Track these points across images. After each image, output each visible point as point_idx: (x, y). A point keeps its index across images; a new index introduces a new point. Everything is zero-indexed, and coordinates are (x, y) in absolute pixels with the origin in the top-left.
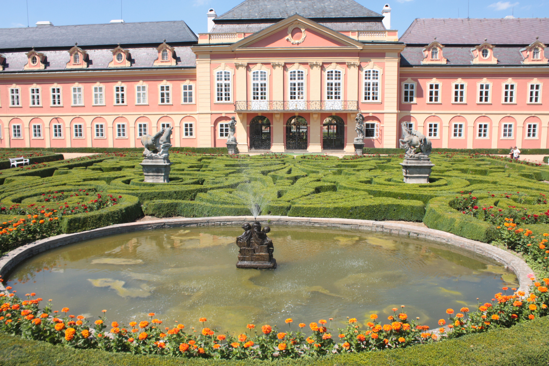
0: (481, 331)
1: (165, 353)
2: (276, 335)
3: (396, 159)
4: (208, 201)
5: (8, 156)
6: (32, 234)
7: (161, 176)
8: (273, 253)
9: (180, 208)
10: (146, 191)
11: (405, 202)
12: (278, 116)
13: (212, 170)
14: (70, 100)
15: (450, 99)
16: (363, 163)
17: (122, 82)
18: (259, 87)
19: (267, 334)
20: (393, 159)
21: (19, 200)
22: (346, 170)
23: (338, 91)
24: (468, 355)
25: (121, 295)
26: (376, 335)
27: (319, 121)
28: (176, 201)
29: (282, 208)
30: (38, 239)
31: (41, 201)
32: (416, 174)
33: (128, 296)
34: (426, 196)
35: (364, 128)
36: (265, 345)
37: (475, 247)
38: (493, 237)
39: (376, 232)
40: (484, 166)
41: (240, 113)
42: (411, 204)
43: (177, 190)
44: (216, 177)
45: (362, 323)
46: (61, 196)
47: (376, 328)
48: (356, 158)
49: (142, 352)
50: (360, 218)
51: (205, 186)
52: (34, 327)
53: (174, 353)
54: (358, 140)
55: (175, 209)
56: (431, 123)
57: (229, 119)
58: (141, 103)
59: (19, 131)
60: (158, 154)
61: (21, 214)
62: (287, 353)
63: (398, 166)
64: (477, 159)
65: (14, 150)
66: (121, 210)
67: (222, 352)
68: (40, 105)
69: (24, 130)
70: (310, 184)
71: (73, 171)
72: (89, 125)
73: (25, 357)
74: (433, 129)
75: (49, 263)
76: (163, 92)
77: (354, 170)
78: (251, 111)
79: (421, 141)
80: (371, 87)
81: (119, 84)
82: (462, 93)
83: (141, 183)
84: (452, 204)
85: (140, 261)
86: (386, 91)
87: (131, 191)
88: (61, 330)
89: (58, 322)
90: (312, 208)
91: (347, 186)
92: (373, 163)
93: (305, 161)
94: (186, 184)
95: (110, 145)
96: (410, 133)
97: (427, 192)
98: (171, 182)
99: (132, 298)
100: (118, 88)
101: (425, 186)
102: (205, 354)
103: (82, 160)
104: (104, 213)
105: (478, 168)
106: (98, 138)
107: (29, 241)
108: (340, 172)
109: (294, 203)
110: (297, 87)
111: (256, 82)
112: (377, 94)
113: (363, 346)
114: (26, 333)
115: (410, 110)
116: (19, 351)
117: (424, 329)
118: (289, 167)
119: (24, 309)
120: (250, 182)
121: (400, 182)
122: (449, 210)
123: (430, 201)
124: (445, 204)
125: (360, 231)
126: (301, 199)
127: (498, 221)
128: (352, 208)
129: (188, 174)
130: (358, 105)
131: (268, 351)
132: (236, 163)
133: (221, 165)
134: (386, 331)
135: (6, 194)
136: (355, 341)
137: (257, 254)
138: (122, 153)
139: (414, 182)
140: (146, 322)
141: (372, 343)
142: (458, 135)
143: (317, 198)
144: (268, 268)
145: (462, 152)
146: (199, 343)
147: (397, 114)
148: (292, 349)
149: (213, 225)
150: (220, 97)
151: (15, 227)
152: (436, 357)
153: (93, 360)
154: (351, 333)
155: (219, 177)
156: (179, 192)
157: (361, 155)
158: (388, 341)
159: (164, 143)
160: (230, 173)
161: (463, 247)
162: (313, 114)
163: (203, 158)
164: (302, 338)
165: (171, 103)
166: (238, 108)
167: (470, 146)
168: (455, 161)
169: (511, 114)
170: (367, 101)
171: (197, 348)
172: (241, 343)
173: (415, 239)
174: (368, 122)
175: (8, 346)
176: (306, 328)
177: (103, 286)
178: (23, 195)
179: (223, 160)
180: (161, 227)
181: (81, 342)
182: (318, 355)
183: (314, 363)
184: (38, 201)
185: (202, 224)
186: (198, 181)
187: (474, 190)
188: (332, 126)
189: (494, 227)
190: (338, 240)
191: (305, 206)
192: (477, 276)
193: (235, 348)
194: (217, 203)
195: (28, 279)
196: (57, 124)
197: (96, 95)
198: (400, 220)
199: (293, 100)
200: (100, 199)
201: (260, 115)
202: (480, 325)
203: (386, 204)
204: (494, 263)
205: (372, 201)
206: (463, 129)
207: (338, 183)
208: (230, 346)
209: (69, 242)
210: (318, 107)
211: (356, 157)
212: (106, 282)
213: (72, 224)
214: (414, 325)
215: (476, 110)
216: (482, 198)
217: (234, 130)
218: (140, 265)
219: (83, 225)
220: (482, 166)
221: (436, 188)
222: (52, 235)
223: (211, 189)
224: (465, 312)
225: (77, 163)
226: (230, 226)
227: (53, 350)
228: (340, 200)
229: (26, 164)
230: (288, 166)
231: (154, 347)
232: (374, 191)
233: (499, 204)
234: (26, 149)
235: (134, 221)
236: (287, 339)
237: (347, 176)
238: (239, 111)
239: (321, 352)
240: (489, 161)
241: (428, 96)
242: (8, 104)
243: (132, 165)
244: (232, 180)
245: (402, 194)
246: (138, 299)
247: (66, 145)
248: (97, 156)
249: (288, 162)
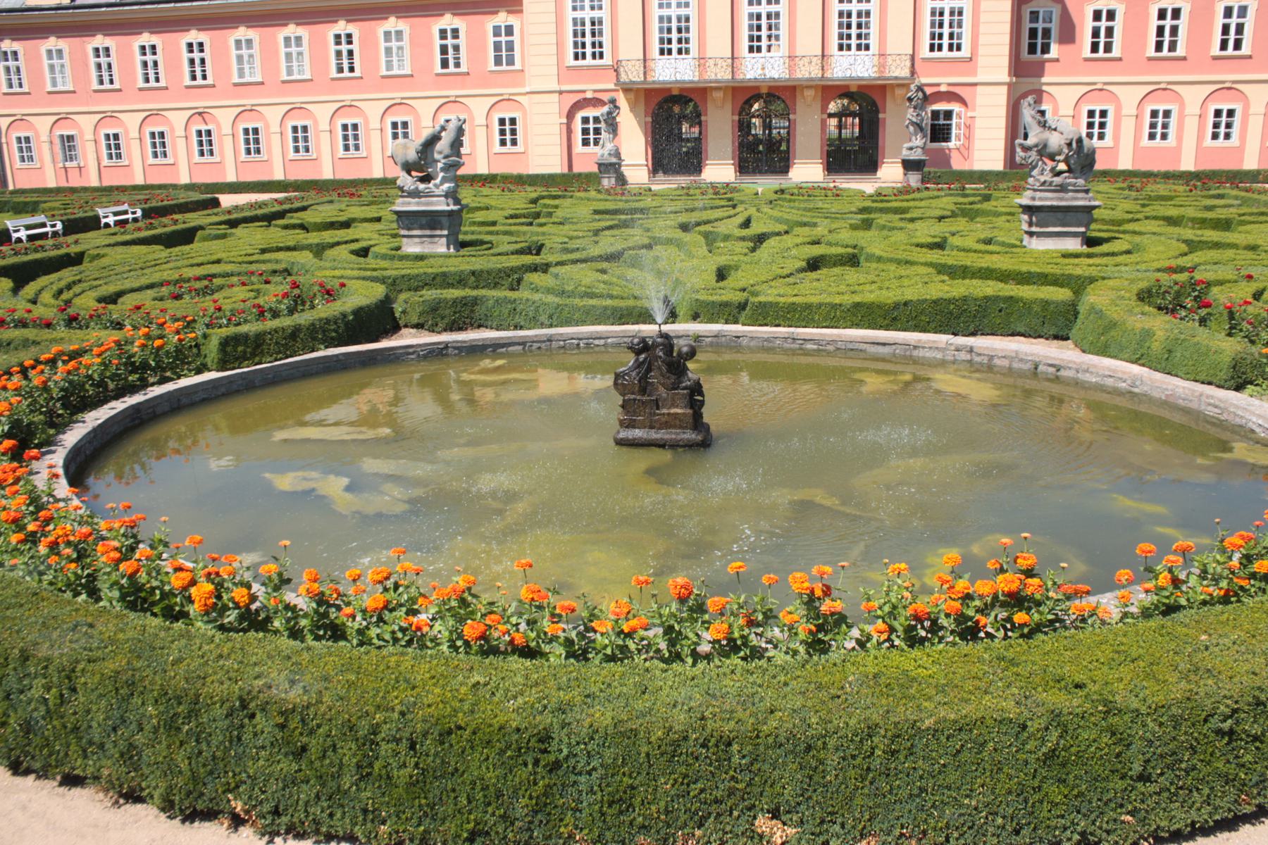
0: (1225, 600)
1: (429, 644)
2: (703, 603)
3: (1003, 193)
4: (549, 291)
5: (95, 204)
6: (136, 373)
7: (441, 236)
9: (484, 308)
10: (403, 272)
11: (1026, 292)
12: (718, 95)
14: (229, 68)
15: (1144, 46)
16: (923, 204)
17: (348, 21)
18: (674, 25)
19: (682, 600)
21: (113, 299)
22: (882, 219)
23: (864, 31)
24: (1195, 660)
25: (339, 509)
26: (957, 604)
27: (818, 105)
28: (475, 293)
29: (725, 305)
30: (153, 384)
31: (161, 299)
33: (358, 512)
34: (1079, 277)
35: (927, 122)
36: (677, 627)
37: (1203, 398)
39: (954, 362)
40: (1225, 211)
41: (628, 89)
42: (1042, 296)
43: (477, 267)
44: (571, 238)
45: (919, 577)
46: (206, 287)
47: (957, 588)
48: (907, 192)
49: (375, 641)
52: (124, 581)
53: (453, 647)
54: (911, 149)
55: (472, 311)
56: (1092, 108)
58: (395, 72)
59: (118, 147)
60: (431, 185)
61: (114, 329)
62: (730, 647)
64: (1205, 193)
65: (110, 190)
66: (344, 315)
67: (569, 642)
68: (162, 83)
69: (128, 146)
70: (794, 252)
71: (239, 231)
72: (275, 128)
73: (99, 648)
74: (1098, 121)
75: (181, 438)
76: (444, 42)
77: (902, 219)
78: (654, 82)
79: (1069, 145)
80: (946, 18)
81: (341, 27)
82: (1174, 30)
83: (395, 254)
84: (1145, 296)
85: (386, 431)
86: (982, 29)
87: (369, 273)
89: (179, 569)
90: (799, 305)
91: (884, 255)
92: (947, 203)
95: (327, 174)
96: (1044, 125)
97: (1081, 268)
98: (464, 251)
99: (367, 516)
100: (338, 37)
101: (1077, 256)
102: (528, 646)
103: (260, 207)
104: (303, 322)
105: (1209, 215)
106: (298, 156)
107: (132, 389)
108: (867, 225)
110: (764, 22)
112: (959, 37)
113: (923, 633)
115: (1041, 75)
116: (86, 633)
117: (1078, 594)
118: (746, 214)
119: (103, 539)
123: (1089, 289)
124: (1127, 295)
125: (916, 361)
126: (773, 284)
128: (896, 306)
129: (506, 233)
130: (913, 65)
131: (684, 642)
132: (621, 205)
133: (584, 211)
134: (981, 597)
136: (902, 619)
137: (665, 411)
139: (1049, 247)
141: (946, 624)
142: (1158, 136)
144: (690, 446)
145: (1168, 178)
146: (514, 620)
147: (1010, 85)
148: (742, 637)
150: (580, 50)
151: (99, 355)
152: (1110, 663)
153: (254, 659)
154: (894, 600)
155: (578, 238)
156: (482, 271)
157: (919, 185)
158: (987, 621)
159: (446, 157)
161: (1171, 400)
164: (771, 610)
165: (463, 69)
166: (623, 78)
167: (1188, 164)
168: (1150, 198)
170: (936, 54)
171: (508, 632)
172: (617, 621)
173: (1049, 380)
174: (936, 107)
175: (64, 622)
177: (299, 488)
178: (123, 288)
179: (589, 200)
180: (438, 352)
181: (231, 617)
182: (808, 653)
183: (798, 673)
184: (155, 299)
185: (536, 345)
186: (529, 248)
187: (1200, 264)
188: (850, 120)
189: (1254, 349)
191: (782, 300)
192: (1206, 469)
193: (602, 634)
194: (571, 295)
196: (203, 128)
197: (289, 56)
198: (1013, 335)
199: (755, 54)
200: (297, 291)
201: (675, 93)
202: (1224, 584)
203: (981, 295)
204: (1251, 439)
206: (1173, 121)
207: (862, 248)
208: (588, 629)
209: (223, 390)
210: (816, 72)
211: (906, 190)
212: (305, 479)
213: (229, 349)
214: (1055, 583)
216: (1220, 283)
217: (613, 127)
218: (385, 441)
219: (254, 349)
220: (1219, 210)
222: (185, 376)
223: (558, 264)
224: (1184, 552)
226: (603, 349)
227: (162, 634)
228: (868, 287)
229: (135, 220)
231: (403, 630)
232: (950, 267)
234: (136, 188)
235: (376, 340)
236: (732, 614)
237: (885, 233)
238: (624, 83)
239: (817, 646)
240: (1236, 198)
241: (1088, 40)
242: (90, 83)
243: (376, 215)
244: (608, 243)
245: (1020, 273)
247: (225, 176)
248: (296, 198)
249: (742, 202)
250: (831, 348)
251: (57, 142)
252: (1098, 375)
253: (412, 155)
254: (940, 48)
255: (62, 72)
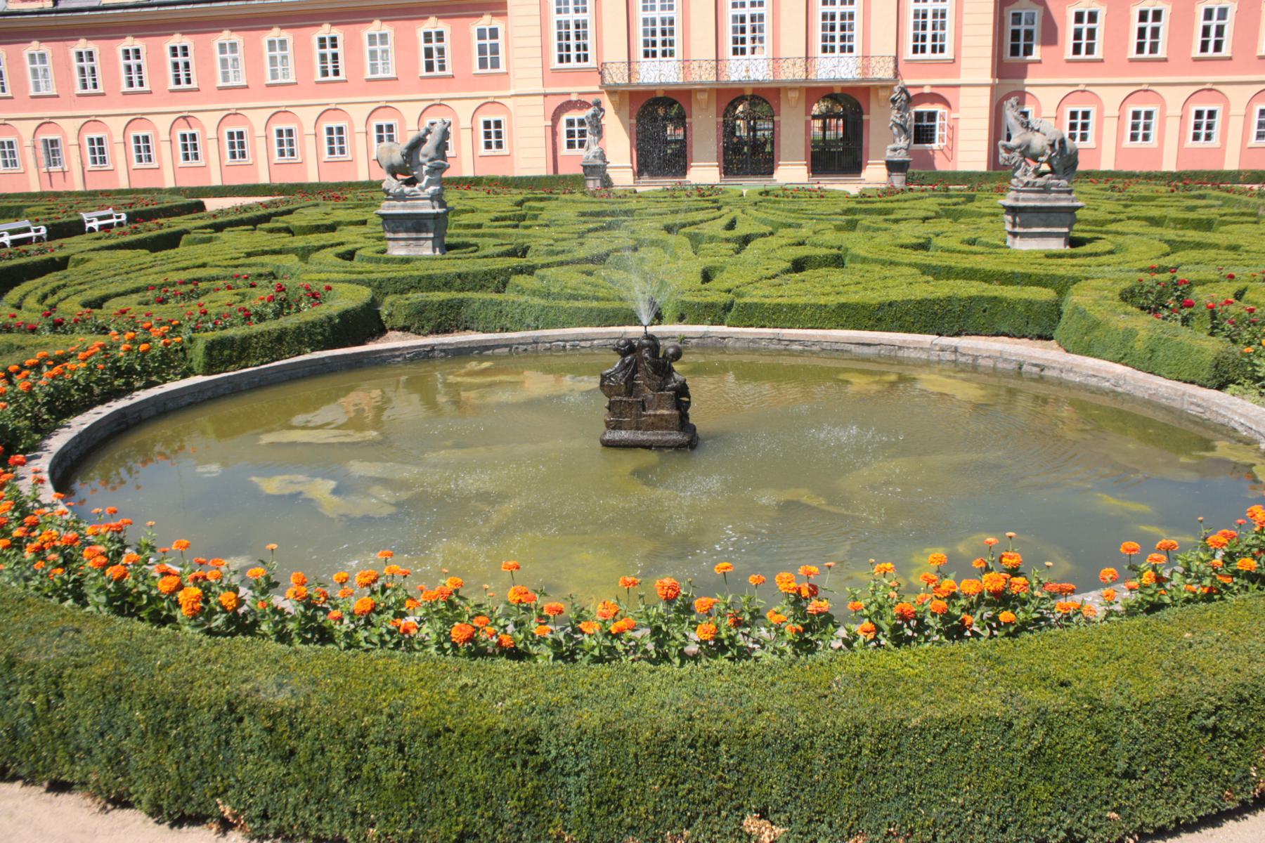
1: (417, 646)
3: (987, 194)
4: (534, 293)
5: (80, 208)
6: (122, 377)
7: (426, 239)
8: (689, 411)
11: (1010, 292)
12: (703, 97)
13: (546, 225)
15: (1126, 48)
16: (907, 205)
18: (658, 27)
19: (669, 601)
20: (979, 195)
21: (98, 303)
22: (866, 220)
23: (847, 33)
26: (943, 604)
27: (802, 107)
28: (461, 295)
30: (138, 389)
31: (147, 304)
32: (1038, 226)
34: (1062, 277)
35: (911, 124)
36: (664, 628)
37: (1186, 398)
38: (1232, 374)
39: (939, 362)
41: (612, 92)
43: (463, 269)
44: (556, 240)
45: (906, 578)
46: (192, 291)
47: (943, 588)
48: (891, 193)
49: (363, 644)
50: (902, 329)
51: (531, 259)
52: (110, 586)
54: (895, 150)
55: (458, 314)
56: (1074, 109)
57: (588, 106)
58: (380, 75)
59: (102, 151)
60: (416, 188)
61: (99, 333)
62: (718, 647)
63: (992, 211)
66: (330, 318)
67: (557, 644)
68: (146, 87)
69: (112, 149)
70: (780, 253)
71: (225, 235)
73: (86, 653)
74: (1080, 122)
76: (428, 45)
77: (886, 220)
78: (638, 85)
79: (1052, 146)
80: (929, 20)
81: (326, 30)
82: (1155, 32)
83: (380, 257)
84: (1128, 296)
86: (965, 30)
87: (354, 277)
88: (172, 593)
89: (166, 573)
92: (931, 204)
93: (769, 201)
94: (485, 257)
95: (312, 177)
96: (1026, 126)
97: (1064, 268)
98: (449, 254)
100: (322, 40)
101: (1060, 256)
102: (515, 648)
104: (289, 326)
105: (1191, 215)
107: (118, 394)
108: (852, 226)
109: (739, 295)
111: (649, 15)
112: (942, 39)
113: (909, 633)
114: (96, 599)
115: (1024, 77)
117: (1063, 593)
118: (731, 216)
120: (635, 249)
121: (1000, 247)
122: (1120, 310)
123: (1072, 289)
124: (1110, 295)
125: (900, 362)
126: (758, 285)
127: (1246, 335)
128: (881, 306)
130: (896, 66)
131: (671, 643)
132: (606, 207)
133: (569, 213)
134: (967, 596)
135: (69, 290)
136: (888, 619)
137: (651, 412)
138: (339, 193)
140: (372, 573)
141: (932, 623)
142: (1140, 137)
143: (797, 282)
146: (501, 622)
147: (993, 86)
148: (730, 637)
149: (547, 350)
150: (564, 53)
151: (84, 360)
153: (242, 662)
154: (880, 600)
155: (564, 240)
156: (468, 274)
157: (903, 186)
158: (972, 620)
160: (590, 231)
161: (1154, 399)
162: (787, 89)
163: (529, 200)
164: (758, 610)
165: (448, 72)
166: (608, 80)
167: (1169, 165)
168: (1132, 199)
169: (1151, 84)
170: (919, 56)
171: (496, 634)
172: (604, 622)
174: (919, 108)
176: (766, 585)
177: (287, 492)
178: (108, 292)
179: (574, 202)
180: (425, 355)
181: (219, 621)
182: (796, 653)
184: (140, 304)
185: (522, 347)
187: (1182, 264)
188: (834, 121)
189: (1235, 349)
190: (848, 382)
191: (768, 301)
192: (1187, 467)
194: (558, 296)
195: (122, 482)
196: (188, 132)
197: (273, 59)
198: (997, 335)
199: (739, 57)
200: (282, 295)
201: (660, 95)
204: (1233, 438)
205: (931, 289)
206: (1155, 122)
207: (847, 249)
208: (575, 631)
209: (209, 394)
210: (800, 74)
211: (890, 191)
212: (292, 482)
213: (215, 353)
214: (1040, 582)
215: (1190, 74)
216: (1202, 283)
218: (372, 443)
220: (1201, 211)
221: (1088, 260)
222: (171, 380)
223: (543, 266)
224: (1168, 550)
225: (233, 218)
226: (589, 351)
227: (150, 638)
228: (852, 288)
229: (120, 224)
230: (727, 215)
231: (391, 633)
232: (934, 268)
233: (1247, 295)
236: (719, 614)
237: (870, 234)
238: (609, 86)
240: (1217, 198)
241: (1070, 42)
242: (73, 87)
243: (361, 218)
244: (595, 245)
245: (1003, 274)
246: (368, 520)
249: (727, 204)
250: (815, 348)
251: (41, 146)
252: (1081, 374)
253: (397, 158)
254: (923, 50)
255: (45, 76)
